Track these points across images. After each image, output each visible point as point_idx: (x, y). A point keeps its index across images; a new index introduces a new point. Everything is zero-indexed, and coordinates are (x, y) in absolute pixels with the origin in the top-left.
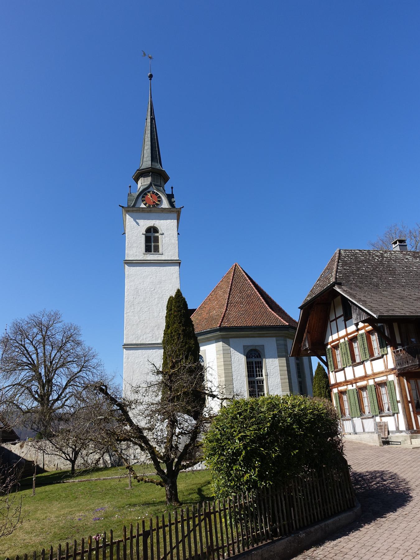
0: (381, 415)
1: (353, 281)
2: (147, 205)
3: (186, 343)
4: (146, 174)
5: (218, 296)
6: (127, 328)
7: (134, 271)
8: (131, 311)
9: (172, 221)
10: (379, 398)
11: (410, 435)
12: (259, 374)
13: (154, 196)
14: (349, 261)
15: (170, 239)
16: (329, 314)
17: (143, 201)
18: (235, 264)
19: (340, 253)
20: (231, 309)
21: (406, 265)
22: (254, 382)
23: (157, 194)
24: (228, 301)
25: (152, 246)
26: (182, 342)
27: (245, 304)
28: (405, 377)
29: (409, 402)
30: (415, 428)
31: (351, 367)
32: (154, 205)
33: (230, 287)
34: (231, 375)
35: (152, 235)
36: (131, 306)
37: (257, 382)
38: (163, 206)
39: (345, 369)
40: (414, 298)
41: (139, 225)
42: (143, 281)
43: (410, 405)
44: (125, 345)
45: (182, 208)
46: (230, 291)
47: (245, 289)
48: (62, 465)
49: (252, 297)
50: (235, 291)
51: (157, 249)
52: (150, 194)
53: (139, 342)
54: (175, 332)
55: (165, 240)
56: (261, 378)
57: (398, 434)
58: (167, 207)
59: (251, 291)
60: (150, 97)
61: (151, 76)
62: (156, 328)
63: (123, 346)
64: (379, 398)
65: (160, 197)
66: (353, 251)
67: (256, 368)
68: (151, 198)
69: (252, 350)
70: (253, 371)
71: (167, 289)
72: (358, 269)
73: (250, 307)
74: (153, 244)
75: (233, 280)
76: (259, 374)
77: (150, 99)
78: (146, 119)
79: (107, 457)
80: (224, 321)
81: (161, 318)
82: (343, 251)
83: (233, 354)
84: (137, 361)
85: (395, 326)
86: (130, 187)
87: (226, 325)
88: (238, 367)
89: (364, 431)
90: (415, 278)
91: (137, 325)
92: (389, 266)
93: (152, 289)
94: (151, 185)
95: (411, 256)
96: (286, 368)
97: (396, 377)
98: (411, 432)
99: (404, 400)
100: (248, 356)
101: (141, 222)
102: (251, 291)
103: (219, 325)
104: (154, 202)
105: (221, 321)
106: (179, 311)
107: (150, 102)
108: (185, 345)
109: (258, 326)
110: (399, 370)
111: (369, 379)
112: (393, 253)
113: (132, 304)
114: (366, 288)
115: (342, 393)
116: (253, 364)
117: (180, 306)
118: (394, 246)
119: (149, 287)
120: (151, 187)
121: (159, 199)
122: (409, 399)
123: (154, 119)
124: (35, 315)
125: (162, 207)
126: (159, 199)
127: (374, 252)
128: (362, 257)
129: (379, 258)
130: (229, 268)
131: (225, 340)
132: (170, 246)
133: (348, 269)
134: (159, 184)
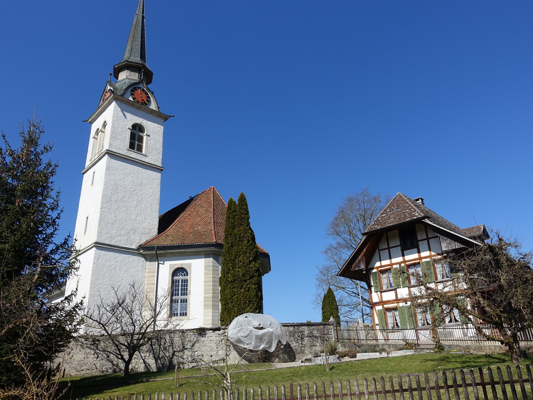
4: (134, 69)
9: (159, 126)
15: (155, 144)
16: (379, 243)
23: (146, 94)
25: (136, 144)
31: (407, 288)
39: (398, 290)
41: (126, 118)
42: (124, 178)
45: (172, 116)
48: (74, 371)
51: (140, 149)
52: (140, 90)
53: (112, 243)
55: (150, 143)
62: (132, 232)
65: (149, 97)
71: (148, 193)
74: (137, 143)
79: (150, 360)
81: (138, 222)
84: (107, 264)
91: (113, 224)
93: (132, 190)
101: (128, 115)
104: (143, 100)
119: (129, 186)
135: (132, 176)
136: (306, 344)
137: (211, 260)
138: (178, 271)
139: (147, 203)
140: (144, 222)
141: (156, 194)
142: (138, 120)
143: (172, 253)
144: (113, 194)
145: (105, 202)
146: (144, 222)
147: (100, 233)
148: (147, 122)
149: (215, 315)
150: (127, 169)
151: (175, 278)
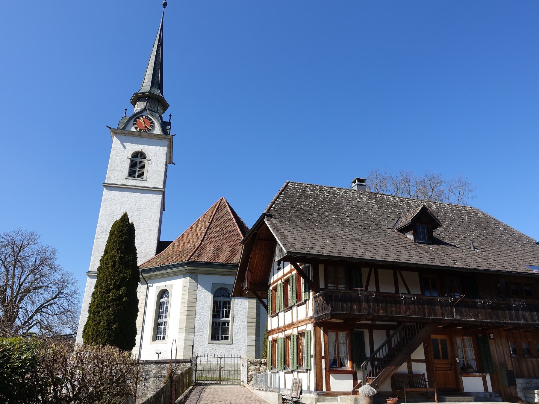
0: (299, 370)
1: (287, 214)
2: (138, 129)
3: (121, 272)
5: (197, 229)
6: (95, 255)
7: (112, 195)
8: (103, 237)
9: (162, 147)
10: (299, 350)
11: (317, 397)
12: (226, 315)
13: (147, 120)
14: (294, 194)
17: (134, 125)
18: (221, 199)
19: (287, 185)
20: (206, 244)
21: (357, 204)
22: (219, 323)
23: (150, 119)
24: (205, 235)
26: (116, 271)
27: (223, 240)
28: (322, 328)
29: (323, 358)
30: (324, 390)
32: (145, 130)
33: (210, 221)
34: (194, 313)
35: (139, 160)
36: (103, 232)
37: (222, 323)
38: (155, 132)
40: (348, 239)
41: (125, 149)
42: (121, 207)
43: (323, 361)
44: (90, 272)
46: (210, 225)
47: (226, 224)
49: (232, 233)
50: (215, 226)
51: (141, 175)
52: (143, 118)
54: (111, 259)
56: (227, 319)
57: (308, 394)
58: (159, 133)
59: (233, 227)
60: (161, 24)
61: (165, 4)
63: (87, 273)
64: (299, 350)
65: (153, 123)
66: (303, 185)
67: (223, 308)
68: (143, 123)
69: (221, 289)
70: (220, 311)
71: (146, 217)
72: (300, 203)
73: (228, 243)
74: (138, 169)
75: (215, 214)
76: (226, 315)
77: (161, 26)
78: (154, 45)
80: (194, 255)
82: (292, 184)
83: (200, 291)
85: (321, 268)
86: (126, 110)
87: (195, 259)
88: (203, 305)
89: (285, 388)
90: (361, 219)
92: (337, 204)
94: (145, 109)
95: (367, 196)
96: (255, 311)
97: (313, 326)
98: (318, 393)
99: (317, 355)
100: (216, 294)
101: (128, 145)
102: (233, 227)
103: (187, 259)
104: (146, 127)
105: (191, 255)
106: (120, 236)
107: (160, 29)
108: (119, 275)
109: (230, 263)
110: (316, 318)
111: (294, 327)
112: (348, 191)
113: (105, 229)
114: (299, 223)
115: (275, 341)
116: (220, 303)
117: (122, 231)
118: (353, 185)
120: (146, 111)
121: (151, 125)
122: (323, 354)
123: (162, 45)
124: (9, 235)
125: (153, 132)
126: (151, 125)
127: (327, 188)
128: (311, 191)
129: (330, 194)
130: (216, 202)
131: (193, 275)
132: (156, 173)
133: (288, 202)
134: (155, 110)
135: (130, 203)
136: (150, 386)
137: (188, 279)
138: (163, 293)
139: (145, 227)
140: (141, 246)
141: (155, 216)
142: (138, 148)
143: (157, 275)
144: (108, 224)
145: (100, 232)
146: (141, 246)
147: (94, 262)
148: (149, 147)
149: (189, 339)
150: (125, 197)
151: (162, 300)
